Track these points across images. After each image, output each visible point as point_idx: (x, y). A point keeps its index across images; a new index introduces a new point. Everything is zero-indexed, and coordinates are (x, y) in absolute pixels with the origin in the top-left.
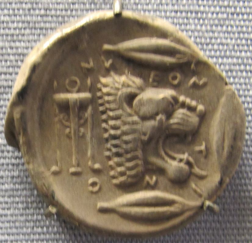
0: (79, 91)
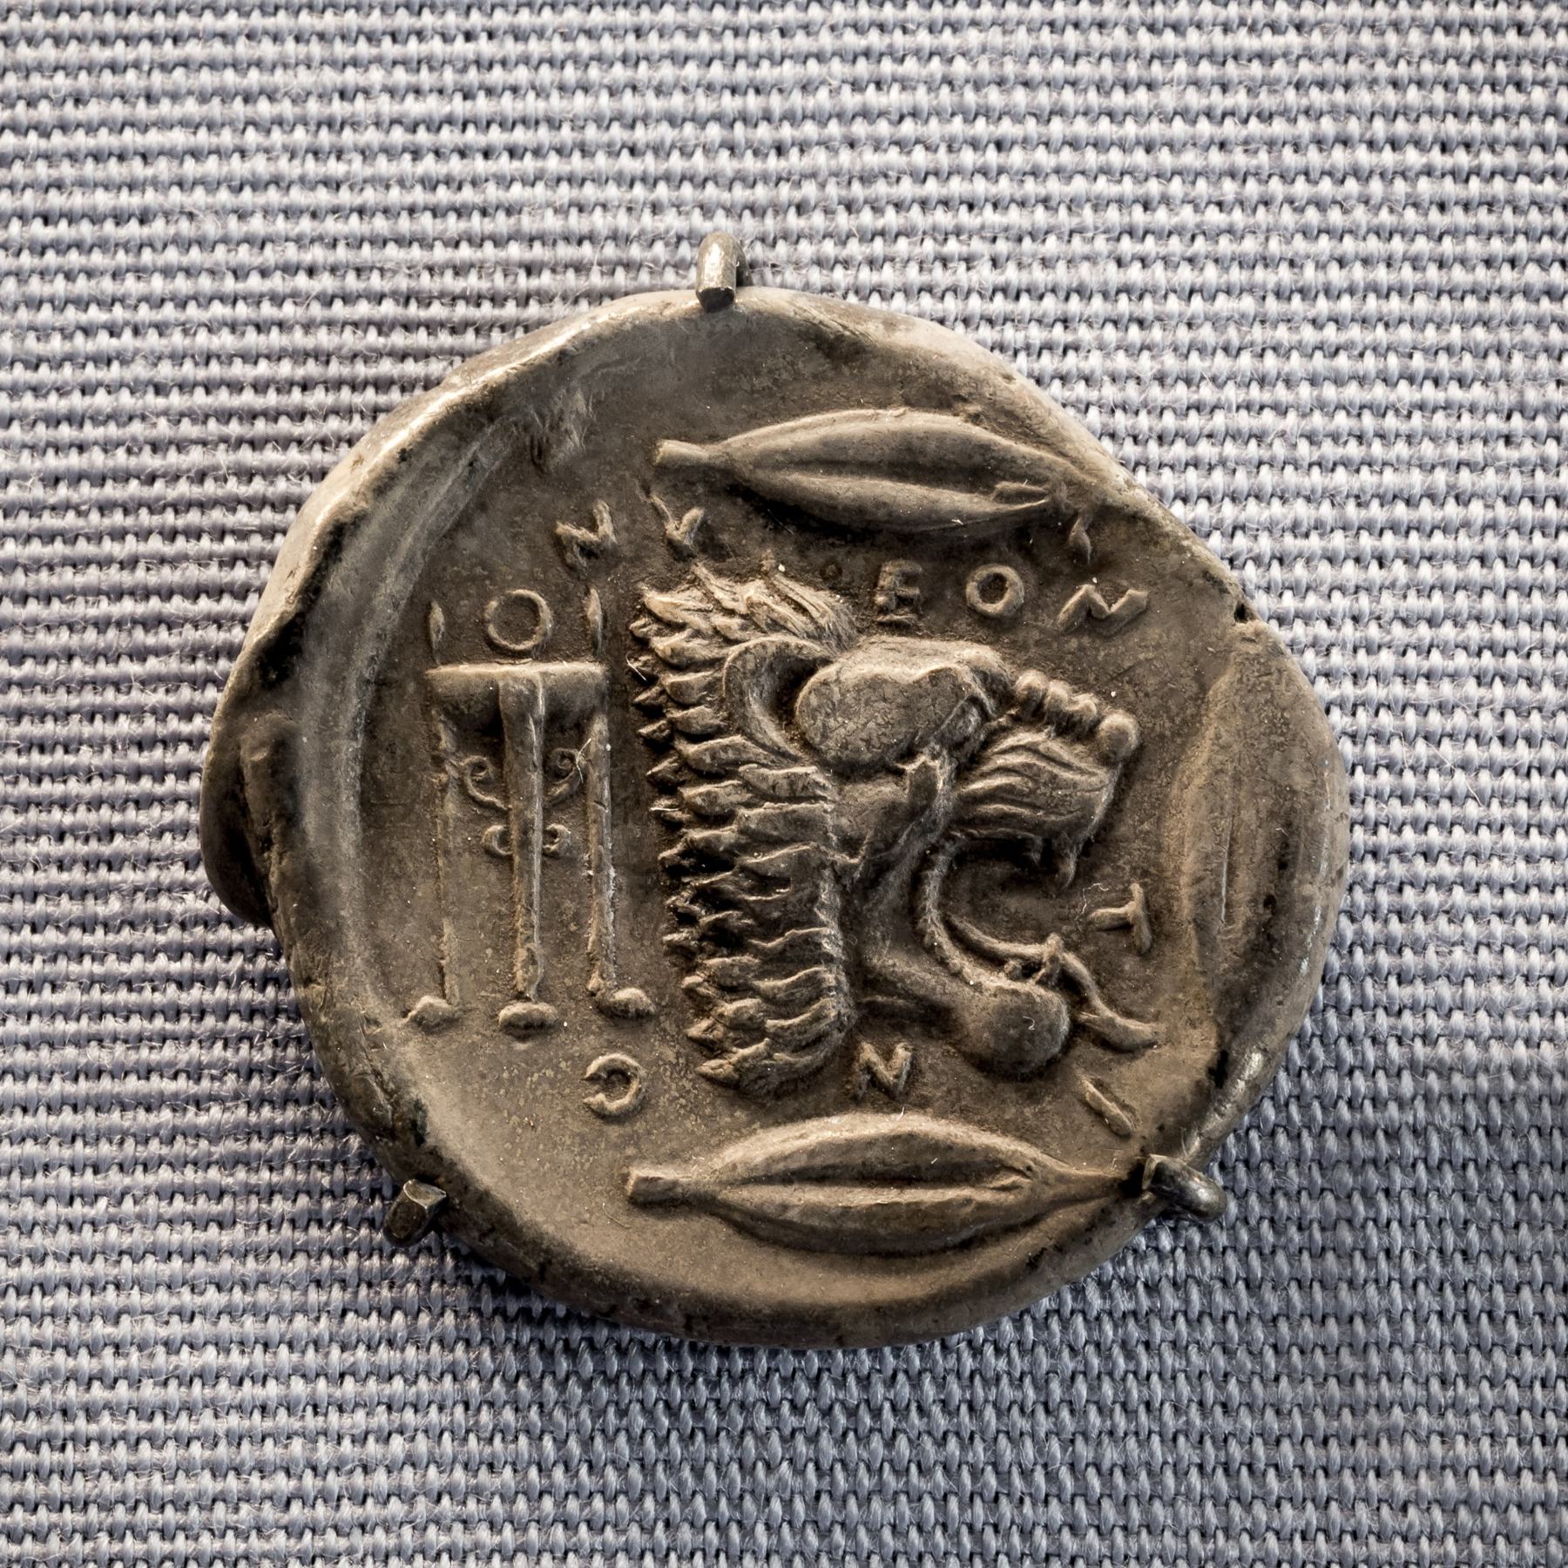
0: (545, 652)
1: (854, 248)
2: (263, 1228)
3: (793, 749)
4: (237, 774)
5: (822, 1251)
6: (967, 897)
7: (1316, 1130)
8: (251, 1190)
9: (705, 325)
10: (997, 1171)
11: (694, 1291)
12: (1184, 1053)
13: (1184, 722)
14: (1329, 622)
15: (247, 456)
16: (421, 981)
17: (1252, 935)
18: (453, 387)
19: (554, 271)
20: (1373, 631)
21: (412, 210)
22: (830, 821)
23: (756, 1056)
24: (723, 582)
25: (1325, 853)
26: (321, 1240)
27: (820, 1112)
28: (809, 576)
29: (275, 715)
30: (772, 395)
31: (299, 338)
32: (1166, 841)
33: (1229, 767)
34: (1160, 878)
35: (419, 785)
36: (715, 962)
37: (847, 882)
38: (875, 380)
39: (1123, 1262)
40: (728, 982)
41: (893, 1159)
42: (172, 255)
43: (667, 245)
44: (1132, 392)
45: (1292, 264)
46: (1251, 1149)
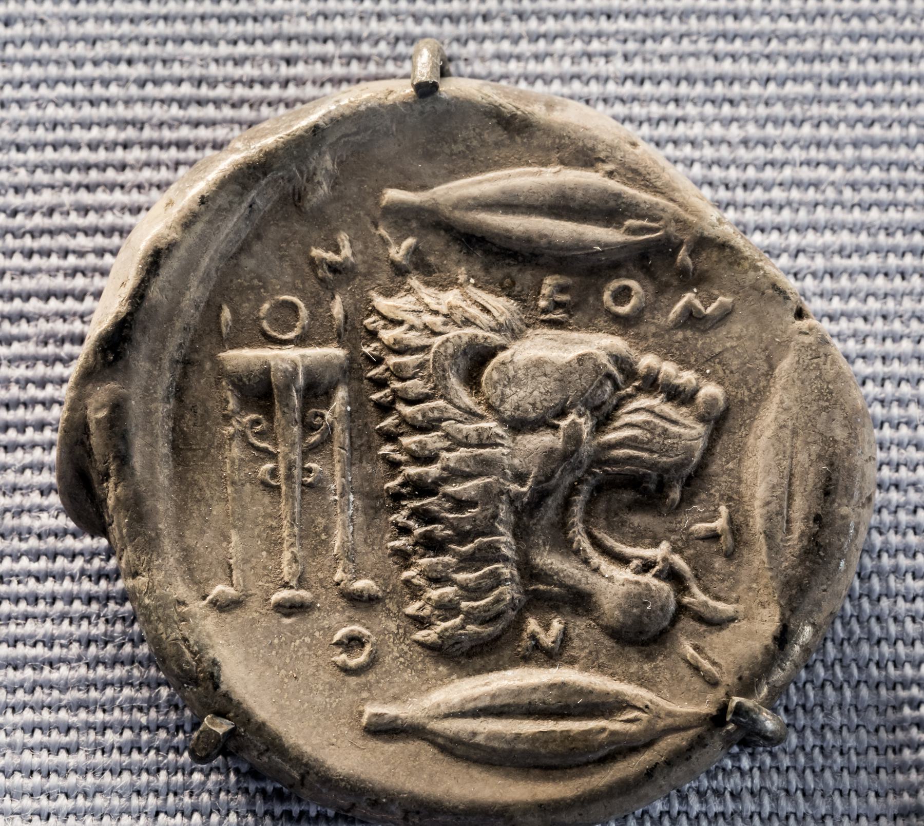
0: (302, 341)
1: (524, 47)
2: (99, 753)
3: (480, 410)
4: (84, 427)
5: (501, 765)
6: (603, 516)
7: (853, 683)
8: (89, 726)
9: (418, 107)
10: (625, 708)
11: (410, 793)
12: (757, 626)
13: (758, 391)
14: (866, 319)
15: (84, 197)
16: (216, 574)
17: (805, 543)
18: (237, 150)
19: (306, 62)
20: (897, 326)
21: (203, 18)
22: (506, 461)
23: (455, 628)
24: (431, 290)
25: (857, 485)
26: (141, 762)
27: (498, 668)
28: (492, 286)
29: (112, 385)
30: (465, 157)
31: (121, 111)
32: (745, 476)
33: (790, 423)
34: (740, 501)
35: (214, 435)
36: (425, 561)
37: (518, 504)
38: (539, 146)
39: (715, 777)
40: (434, 574)
41: (550, 700)
42: (28, 50)
43: (389, 43)
44: (724, 152)
45: (841, 59)
46: (806, 697)
